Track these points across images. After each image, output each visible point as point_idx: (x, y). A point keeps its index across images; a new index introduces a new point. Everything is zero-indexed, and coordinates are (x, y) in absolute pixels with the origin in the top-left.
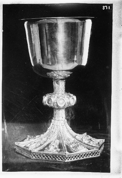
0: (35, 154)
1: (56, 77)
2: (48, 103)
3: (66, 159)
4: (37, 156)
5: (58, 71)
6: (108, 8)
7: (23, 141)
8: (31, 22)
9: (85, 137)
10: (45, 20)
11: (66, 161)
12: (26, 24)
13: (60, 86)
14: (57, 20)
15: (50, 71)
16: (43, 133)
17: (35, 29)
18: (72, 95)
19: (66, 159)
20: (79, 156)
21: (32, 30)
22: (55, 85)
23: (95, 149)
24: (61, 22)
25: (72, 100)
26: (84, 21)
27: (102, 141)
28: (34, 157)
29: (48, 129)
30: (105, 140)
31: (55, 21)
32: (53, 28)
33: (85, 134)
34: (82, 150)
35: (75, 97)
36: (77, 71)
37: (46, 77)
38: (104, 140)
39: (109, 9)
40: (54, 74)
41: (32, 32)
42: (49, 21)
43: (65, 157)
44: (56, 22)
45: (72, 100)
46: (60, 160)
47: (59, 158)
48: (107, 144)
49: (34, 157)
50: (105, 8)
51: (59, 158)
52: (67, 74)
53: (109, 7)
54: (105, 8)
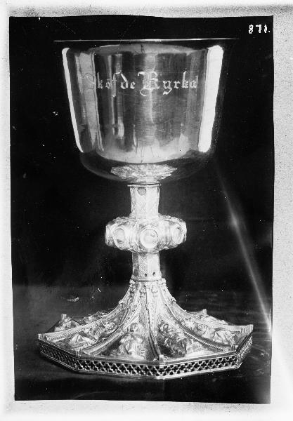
0: (89, 362)
1: (136, 178)
2: (144, 239)
3: (159, 373)
4: (138, 369)
5: (141, 164)
6: (263, 28)
7: (52, 330)
8: (76, 49)
9: (207, 323)
10: (107, 49)
11: (158, 378)
12: (65, 51)
13: (145, 202)
14: (142, 46)
15: (121, 164)
16: (108, 311)
17: (86, 61)
18: (175, 220)
19: (159, 373)
20: (199, 366)
21: (77, 64)
22: (135, 194)
23: (226, 350)
24: (152, 52)
25: (118, 234)
26: (204, 49)
27: (250, 328)
28: (129, 373)
29: (121, 302)
30: (254, 330)
31: (135, 49)
32: (132, 65)
33: (204, 311)
34: (196, 353)
35: (184, 226)
36: (188, 167)
37: (108, 177)
38: (250, 328)
39: (265, 31)
40: (132, 172)
41: (78, 68)
42: (127, 49)
43: (158, 368)
44: (140, 52)
45: (175, 232)
46: (91, 370)
47: (135, 371)
48: (260, 335)
49: (129, 373)
50: (256, 29)
51: (135, 371)
52: (166, 172)
53: (265, 26)
54: (256, 29)
